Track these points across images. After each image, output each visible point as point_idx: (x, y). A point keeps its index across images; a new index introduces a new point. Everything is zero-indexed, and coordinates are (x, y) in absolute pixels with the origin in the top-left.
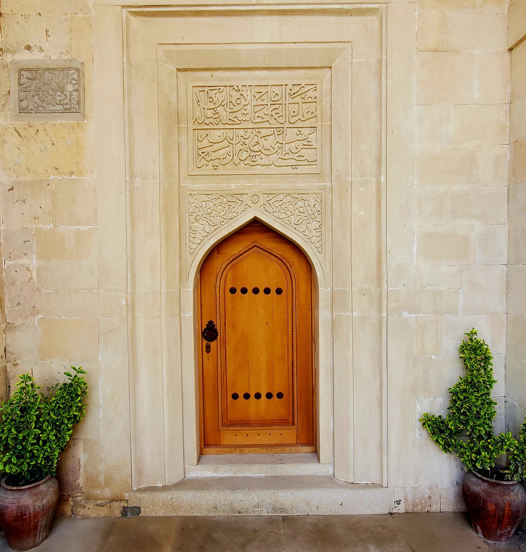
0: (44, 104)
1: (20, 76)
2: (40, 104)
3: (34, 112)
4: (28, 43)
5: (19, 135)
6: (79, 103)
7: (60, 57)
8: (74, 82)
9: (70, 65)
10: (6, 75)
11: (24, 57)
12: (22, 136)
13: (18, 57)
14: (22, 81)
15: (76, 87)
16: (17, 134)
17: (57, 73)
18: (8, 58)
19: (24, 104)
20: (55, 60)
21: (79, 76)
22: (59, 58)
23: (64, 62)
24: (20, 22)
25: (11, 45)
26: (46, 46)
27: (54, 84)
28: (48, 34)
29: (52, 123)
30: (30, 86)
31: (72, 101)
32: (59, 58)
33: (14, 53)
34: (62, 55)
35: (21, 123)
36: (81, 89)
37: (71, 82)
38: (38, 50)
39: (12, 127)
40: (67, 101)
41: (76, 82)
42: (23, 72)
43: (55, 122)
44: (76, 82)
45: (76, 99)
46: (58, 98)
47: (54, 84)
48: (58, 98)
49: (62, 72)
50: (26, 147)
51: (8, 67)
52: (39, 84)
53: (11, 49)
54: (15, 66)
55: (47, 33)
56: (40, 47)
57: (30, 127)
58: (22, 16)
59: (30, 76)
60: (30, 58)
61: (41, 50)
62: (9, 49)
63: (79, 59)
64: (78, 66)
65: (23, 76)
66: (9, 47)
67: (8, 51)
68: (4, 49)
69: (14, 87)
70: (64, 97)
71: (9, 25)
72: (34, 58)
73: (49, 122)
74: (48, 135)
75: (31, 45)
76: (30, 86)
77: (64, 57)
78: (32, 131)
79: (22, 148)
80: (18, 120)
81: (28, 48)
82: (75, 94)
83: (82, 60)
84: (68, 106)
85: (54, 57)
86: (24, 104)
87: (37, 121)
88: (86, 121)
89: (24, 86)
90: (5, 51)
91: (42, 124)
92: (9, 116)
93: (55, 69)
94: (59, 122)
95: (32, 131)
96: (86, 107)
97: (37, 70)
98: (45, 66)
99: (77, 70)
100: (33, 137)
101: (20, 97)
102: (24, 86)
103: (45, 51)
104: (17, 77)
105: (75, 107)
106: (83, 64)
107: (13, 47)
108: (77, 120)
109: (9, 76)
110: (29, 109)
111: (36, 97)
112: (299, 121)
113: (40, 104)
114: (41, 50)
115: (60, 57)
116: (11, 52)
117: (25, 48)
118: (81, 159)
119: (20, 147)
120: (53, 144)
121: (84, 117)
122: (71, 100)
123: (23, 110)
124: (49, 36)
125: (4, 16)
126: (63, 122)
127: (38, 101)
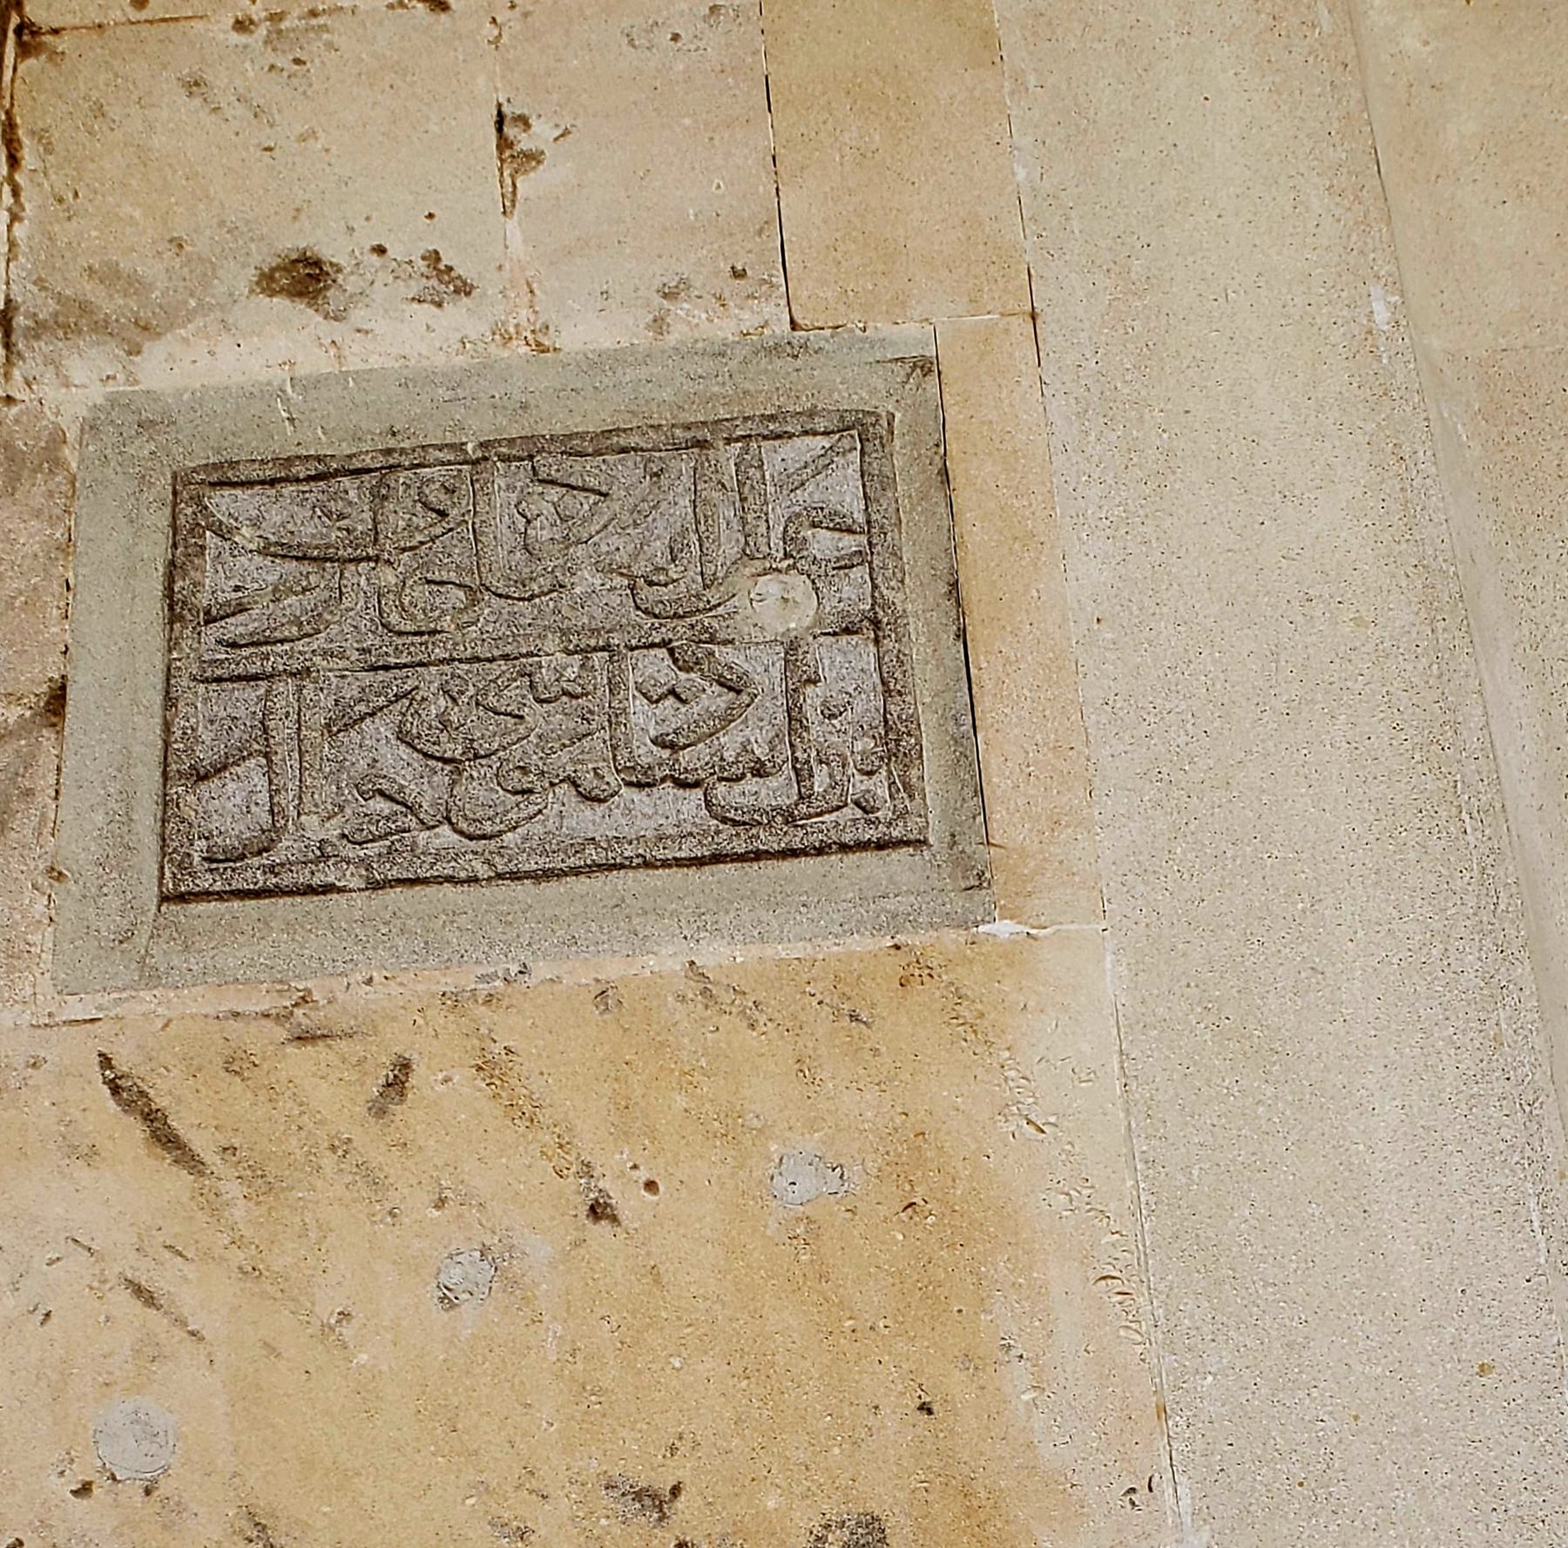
0: (478, 790)
1: (188, 538)
2: (428, 790)
3: (353, 879)
4: (292, 241)
5: (165, 1138)
6: (895, 744)
7: (659, 324)
8: (823, 543)
9: (769, 387)
10: (32, 537)
11: (244, 363)
12: (201, 1143)
13: (174, 369)
14: (211, 583)
15: (852, 590)
16: (136, 1130)
17: (627, 471)
18: (69, 386)
19: (231, 806)
20: (597, 363)
21: (873, 484)
22: (644, 339)
23: (706, 366)
24: (219, 79)
25: (108, 275)
26: (493, 244)
27: (587, 579)
28: (524, 142)
29: (580, 974)
30: (311, 625)
31: (817, 729)
32: (644, 339)
33: (138, 333)
34: (680, 309)
35: (199, 1002)
36: (917, 606)
37: (793, 548)
38: (414, 288)
39: (80, 1051)
40: (755, 733)
41: (850, 543)
42: (222, 503)
43: (612, 969)
44: (850, 543)
45: (867, 705)
46: (644, 719)
47: (587, 579)
48: (644, 719)
49: (683, 465)
50: (251, 1272)
51: (57, 463)
52: (420, 593)
53: (109, 304)
54: (142, 448)
55: (504, 143)
56: (435, 257)
57: (303, 1038)
58: (241, 25)
59: (309, 531)
60: (315, 362)
61: (445, 281)
62: (85, 308)
63: (882, 327)
64: (847, 386)
65: (223, 533)
66: (92, 291)
67: (74, 321)
68: (33, 304)
69: (116, 644)
70: (715, 700)
71: (99, 111)
72: (360, 356)
73: (542, 970)
74: (525, 1114)
75: (331, 250)
76: (311, 625)
77: (694, 322)
78: (328, 1088)
79: (199, 1292)
80: (151, 977)
81: (305, 278)
82: (846, 666)
83: (909, 336)
84: (776, 791)
85: (583, 333)
86: (231, 806)
87: (382, 967)
88: (1004, 928)
89: (235, 627)
90: (39, 329)
91: (454, 1001)
92: (43, 938)
93: (605, 443)
94: (666, 959)
95: (328, 1088)
96: (997, 780)
97: (380, 473)
98: (476, 429)
99: (861, 431)
100: (341, 1147)
101: (190, 735)
102: (235, 627)
103: (489, 285)
104: (155, 549)
105: (857, 792)
106: (925, 367)
107: (136, 285)
108: (896, 922)
109: (67, 547)
110: (286, 849)
111: (381, 729)
112: (671, 699)
113: (428, 790)
114: (445, 281)
115: (659, 324)
116: (103, 328)
117: (267, 282)
118: (969, 1361)
119: (158, 1281)
120: (599, 1211)
121: (982, 881)
122: (795, 718)
123: (206, 877)
124: (534, 157)
125: (62, 44)
126: (714, 954)
127: (399, 765)
